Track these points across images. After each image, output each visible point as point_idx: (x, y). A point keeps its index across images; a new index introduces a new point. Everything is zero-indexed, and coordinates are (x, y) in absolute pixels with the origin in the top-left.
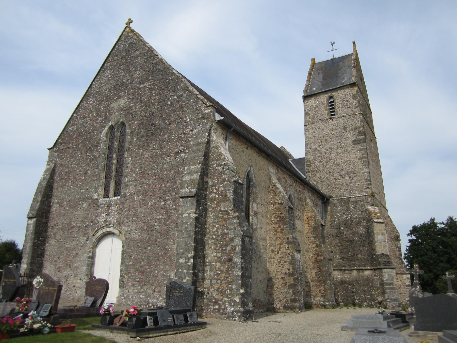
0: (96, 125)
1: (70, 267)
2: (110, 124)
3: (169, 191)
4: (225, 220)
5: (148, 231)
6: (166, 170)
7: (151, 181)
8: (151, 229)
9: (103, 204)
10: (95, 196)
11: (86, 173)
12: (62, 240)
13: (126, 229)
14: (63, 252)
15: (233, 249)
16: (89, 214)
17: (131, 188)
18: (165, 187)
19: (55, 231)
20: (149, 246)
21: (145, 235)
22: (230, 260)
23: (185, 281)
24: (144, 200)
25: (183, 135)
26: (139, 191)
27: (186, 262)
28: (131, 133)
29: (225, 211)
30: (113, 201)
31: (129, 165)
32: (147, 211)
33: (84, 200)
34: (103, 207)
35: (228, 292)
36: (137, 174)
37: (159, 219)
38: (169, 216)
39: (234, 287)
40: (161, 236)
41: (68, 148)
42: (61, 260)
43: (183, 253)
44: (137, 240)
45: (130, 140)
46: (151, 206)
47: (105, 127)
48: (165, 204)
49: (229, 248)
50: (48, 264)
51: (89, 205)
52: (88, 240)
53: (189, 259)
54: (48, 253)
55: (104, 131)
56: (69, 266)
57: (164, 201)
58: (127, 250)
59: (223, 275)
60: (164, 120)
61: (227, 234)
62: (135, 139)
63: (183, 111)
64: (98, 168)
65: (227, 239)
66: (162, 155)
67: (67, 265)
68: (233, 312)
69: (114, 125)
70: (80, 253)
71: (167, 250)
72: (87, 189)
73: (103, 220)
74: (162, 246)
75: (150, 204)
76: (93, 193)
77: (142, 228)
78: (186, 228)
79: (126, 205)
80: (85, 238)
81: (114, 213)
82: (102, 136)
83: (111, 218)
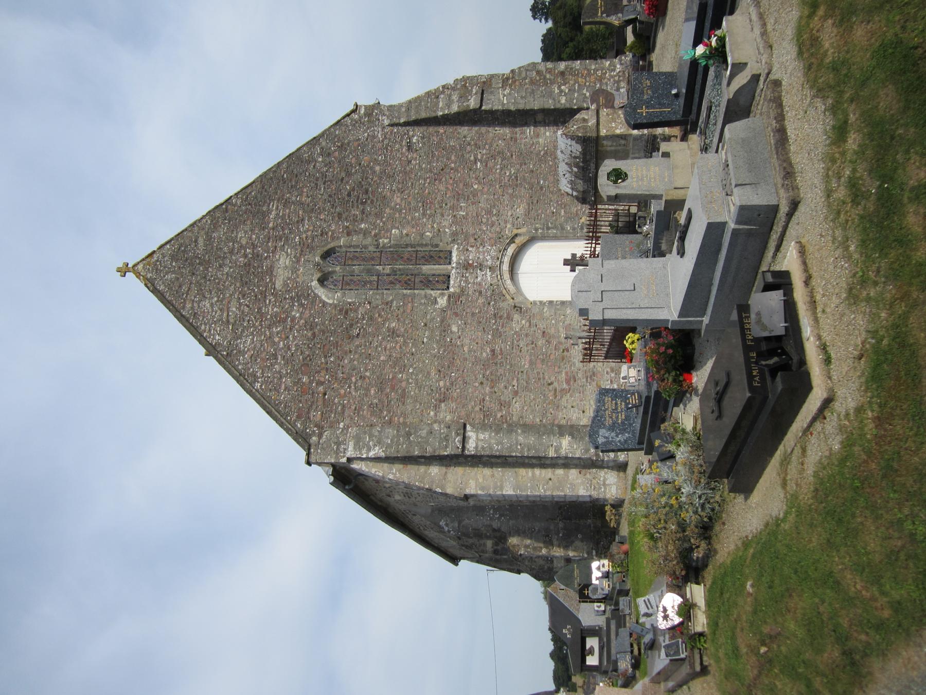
0: (302, 321)
1: (568, 351)
2: (315, 283)
3: (463, 155)
4: (514, 82)
5: (517, 186)
6: (429, 163)
7: (442, 187)
8: (515, 182)
9: (460, 281)
10: (442, 302)
11: (393, 333)
12: (515, 383)
13: (509, 226)
14: (538, 373)
15: (549, 71)
16: (473, 314)
17: (445, 223)
18: (455, 163)
19: (495, 407)
20: (539, 183)
21: (523, 190)
22: (562, 73)
23: (588, 94)
24: (468, 197)
25: (386, 142)
26: (453, 208)
27: (566, 95)
28: (349, 234)
29: (503, 82)
30: (460, 259)
31: (405, 232)
32: (486, 190)
33: (445, 328)
34: (467, 281)
35: (599, 73)
36: (424, 214)
37: (501, 169)
38: (499, 153)
39: (593, 67)
40: (525, 164)
41: (325, 394)
42: (553, 379)
43: (554, 99)
44: (529, 204)
45: (361, 236)
46: (479, 183)
47: (316, 296)
48: (481, 161)
49: (548, 76)
50: (560, 415)
51: (456, 314)
52: (521, 308)
53: (561, 91)
54: (538, 420)
55: (323, 297)
56: (565, 353)
57: (476, 163)
58: (542, 221)
59: (580, 80)
60: (349, 174)
61: (531, 79)
62: (363, 226)
63: (349, 143)
64: (392, 301)
65: (538, 78)
66: (406, 173)
67: (563, 359)
68: (621, 64)
69: (319, 275)
70: (542, 326)
71: (546, 153)
72: (426, 325)
73: (489, 273)
74: (540, 160)
75: (476, 187)
76: (435, 310)
77: (512, 196)
78: (522, 97)
79: (471, 231)
80: (516, 317)
81: (479, 253)
82: (331, 301)
83: (488, 257)
